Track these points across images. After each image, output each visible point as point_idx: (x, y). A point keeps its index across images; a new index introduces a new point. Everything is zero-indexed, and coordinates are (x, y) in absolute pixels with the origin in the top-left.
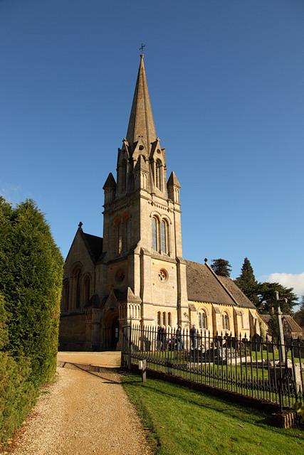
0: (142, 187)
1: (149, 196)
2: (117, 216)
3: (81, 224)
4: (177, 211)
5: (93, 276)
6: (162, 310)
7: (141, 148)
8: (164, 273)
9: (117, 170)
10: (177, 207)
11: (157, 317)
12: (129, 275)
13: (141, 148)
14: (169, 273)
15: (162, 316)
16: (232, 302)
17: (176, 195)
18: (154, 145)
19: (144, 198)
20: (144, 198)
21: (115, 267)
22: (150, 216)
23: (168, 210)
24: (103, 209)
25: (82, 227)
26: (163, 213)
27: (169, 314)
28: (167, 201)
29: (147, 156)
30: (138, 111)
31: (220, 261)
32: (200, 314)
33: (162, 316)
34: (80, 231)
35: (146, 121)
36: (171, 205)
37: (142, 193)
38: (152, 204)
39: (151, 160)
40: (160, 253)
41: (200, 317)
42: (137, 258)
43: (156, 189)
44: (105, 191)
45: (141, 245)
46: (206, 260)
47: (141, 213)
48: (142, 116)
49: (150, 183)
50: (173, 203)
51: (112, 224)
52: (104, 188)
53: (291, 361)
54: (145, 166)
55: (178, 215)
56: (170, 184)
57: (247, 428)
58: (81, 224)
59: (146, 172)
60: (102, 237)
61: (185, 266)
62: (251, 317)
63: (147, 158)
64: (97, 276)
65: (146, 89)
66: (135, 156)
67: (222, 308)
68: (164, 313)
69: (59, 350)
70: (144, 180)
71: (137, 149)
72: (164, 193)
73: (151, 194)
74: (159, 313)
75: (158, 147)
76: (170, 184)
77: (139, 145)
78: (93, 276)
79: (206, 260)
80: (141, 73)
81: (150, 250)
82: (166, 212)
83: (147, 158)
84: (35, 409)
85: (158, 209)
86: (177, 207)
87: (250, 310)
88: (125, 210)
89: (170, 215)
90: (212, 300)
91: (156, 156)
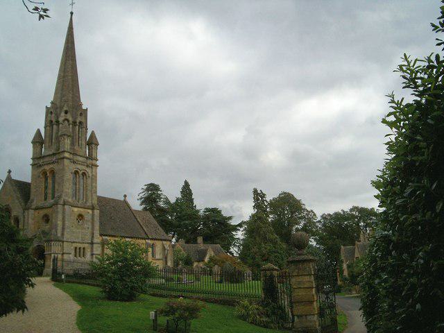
3: (10, 172)
5: (22, 219)
6: (79, 245)
8: (81, 217)
9: (45, 128)
11: (74, 251)
12: (54, 220)
15: (78, 250)
16: (145, 236)
21: (42, 212)
23: (87, 166)
27: (84, 248)
31: (152, 185)
33: (78, 250)
51: (39, 176)
57: (264, 329)
58: (10, 172)
60: (30, 182)
62: (164, 248)
63: (71, 122)
64: (26, 219)
68: (80, 248)
69: (29, 184)
74: (76, 248)
78: (22, 219)
81: (70, 200)
82: (84, 168)
84: (362, 311)
87: (164, 242)
88: (51, 166)
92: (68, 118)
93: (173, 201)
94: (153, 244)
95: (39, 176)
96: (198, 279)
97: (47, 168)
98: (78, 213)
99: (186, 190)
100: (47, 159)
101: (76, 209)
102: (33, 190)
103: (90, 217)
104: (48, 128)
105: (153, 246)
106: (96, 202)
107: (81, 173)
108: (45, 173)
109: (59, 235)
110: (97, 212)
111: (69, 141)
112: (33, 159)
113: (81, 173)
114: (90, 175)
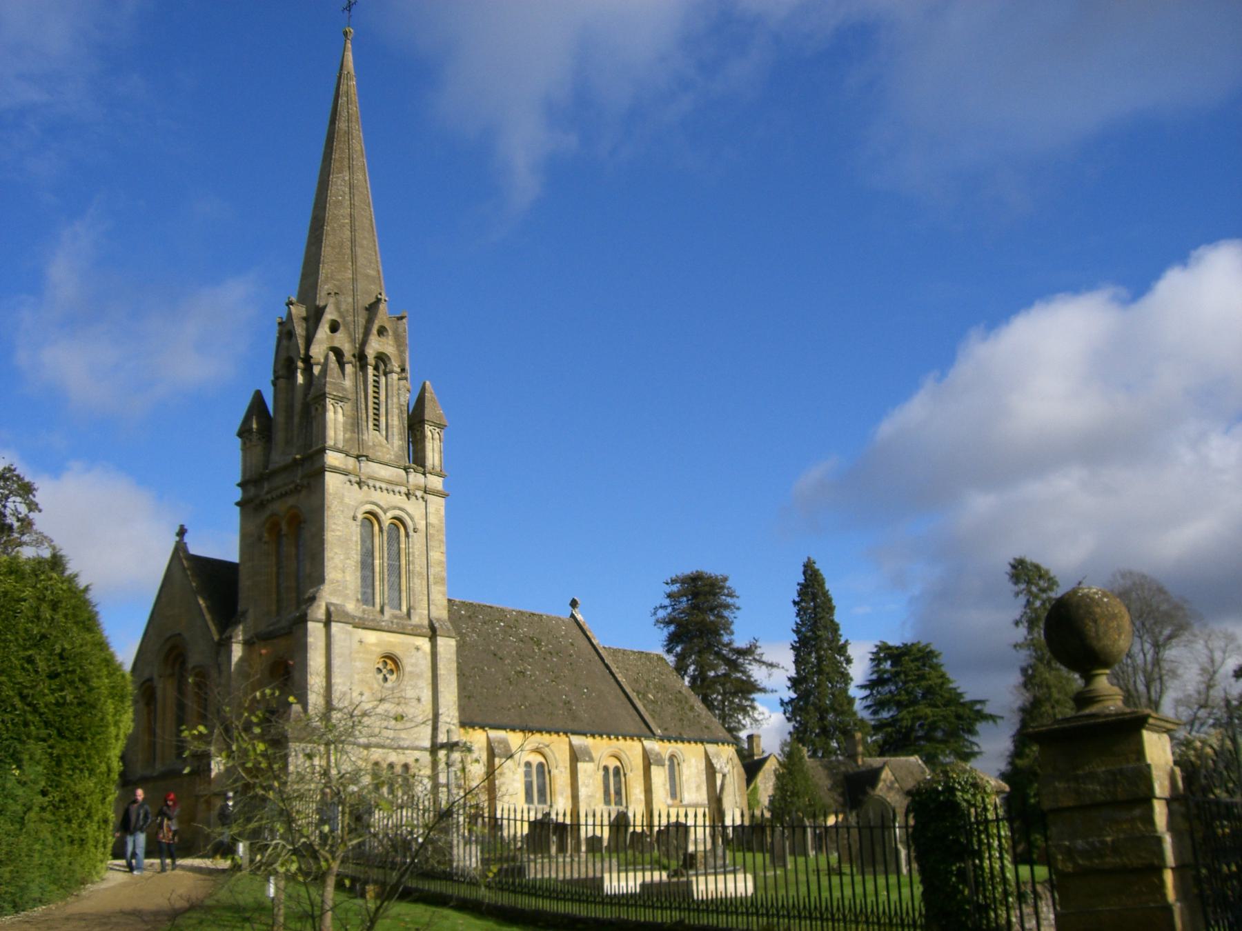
0: (330, 442)
1: (351, 463)
2: (273, 515)
3: (182, 532)
4: (436, 493)
7: (334, 328)
8: (391, 662)
9: (274, 384)
10: (436, 482)
13: (334, 328)
14: (408, 663)
17: (433, 453)
18: (372, 309)
19: (335, 470)
20: (335, 470)
22: (354, 518)
23: (408, 495)
24: (238, 494)
25: (187, 539)
26: (389, 502)
28: (406, 469)
29: (348, 349)
30: (330, 212)
32: (606, 769)
34: (180, 550)
35: (353, 241)
36: (416, 479)
37: (332, 458)
38: (360, 484)
39: (361, 358)
40: (382, 611)
41: (528, 774)
42: (315, 630)
43: (371, 436)
44: (244, 444)
45: (328, 596)
46: (574, 604)
47: (327, 513)
48: (343, 225)
49: (355, 425)
50: (424, 474)
52: (240, 434)
53: (616, 864)
54: (344, 381)
55: (437, 504)
56: (415, 424)
58: (182, 532)
59: (341, 399)
61: (453, 642)
62: (711, 770)
65: (356, 141)
66: (318, 351)
67: (601, 748)
70: (336, 418)
71: (323, 332)
72: (397, 442)
73: (358, 457)
75: (384, 315)
76: (415, 424)
77: (329, 316)
79: (574, 604)
80: (343, 88)
82: (400, 500)
83: (348, 356)
85: (377, 496)
86: (436, 482)
87: (711, 748)
88: (291, 501)
89: (414, 509)
90: (571, 725)
91: (375, 346)
92: (337, 344)
93: (797, 639)
94: (672, 757)
95: (260, 538)
96: (467, 842)
97: (280, 507)
98: (379, 651)
99: (798, 584)
100: (279, 481)
101: (371, 637)
102: (245, 582)
103: (426, 664)
104: (282, 382)
105: (673, 763)
106: (444, 614)
107: (386, 519)
108: (274, 528)
109: (976, 847)
110: (447, 646)
111: (340, 418)
112: (242, 485)
113: (386, 519)
114: (421, 525)
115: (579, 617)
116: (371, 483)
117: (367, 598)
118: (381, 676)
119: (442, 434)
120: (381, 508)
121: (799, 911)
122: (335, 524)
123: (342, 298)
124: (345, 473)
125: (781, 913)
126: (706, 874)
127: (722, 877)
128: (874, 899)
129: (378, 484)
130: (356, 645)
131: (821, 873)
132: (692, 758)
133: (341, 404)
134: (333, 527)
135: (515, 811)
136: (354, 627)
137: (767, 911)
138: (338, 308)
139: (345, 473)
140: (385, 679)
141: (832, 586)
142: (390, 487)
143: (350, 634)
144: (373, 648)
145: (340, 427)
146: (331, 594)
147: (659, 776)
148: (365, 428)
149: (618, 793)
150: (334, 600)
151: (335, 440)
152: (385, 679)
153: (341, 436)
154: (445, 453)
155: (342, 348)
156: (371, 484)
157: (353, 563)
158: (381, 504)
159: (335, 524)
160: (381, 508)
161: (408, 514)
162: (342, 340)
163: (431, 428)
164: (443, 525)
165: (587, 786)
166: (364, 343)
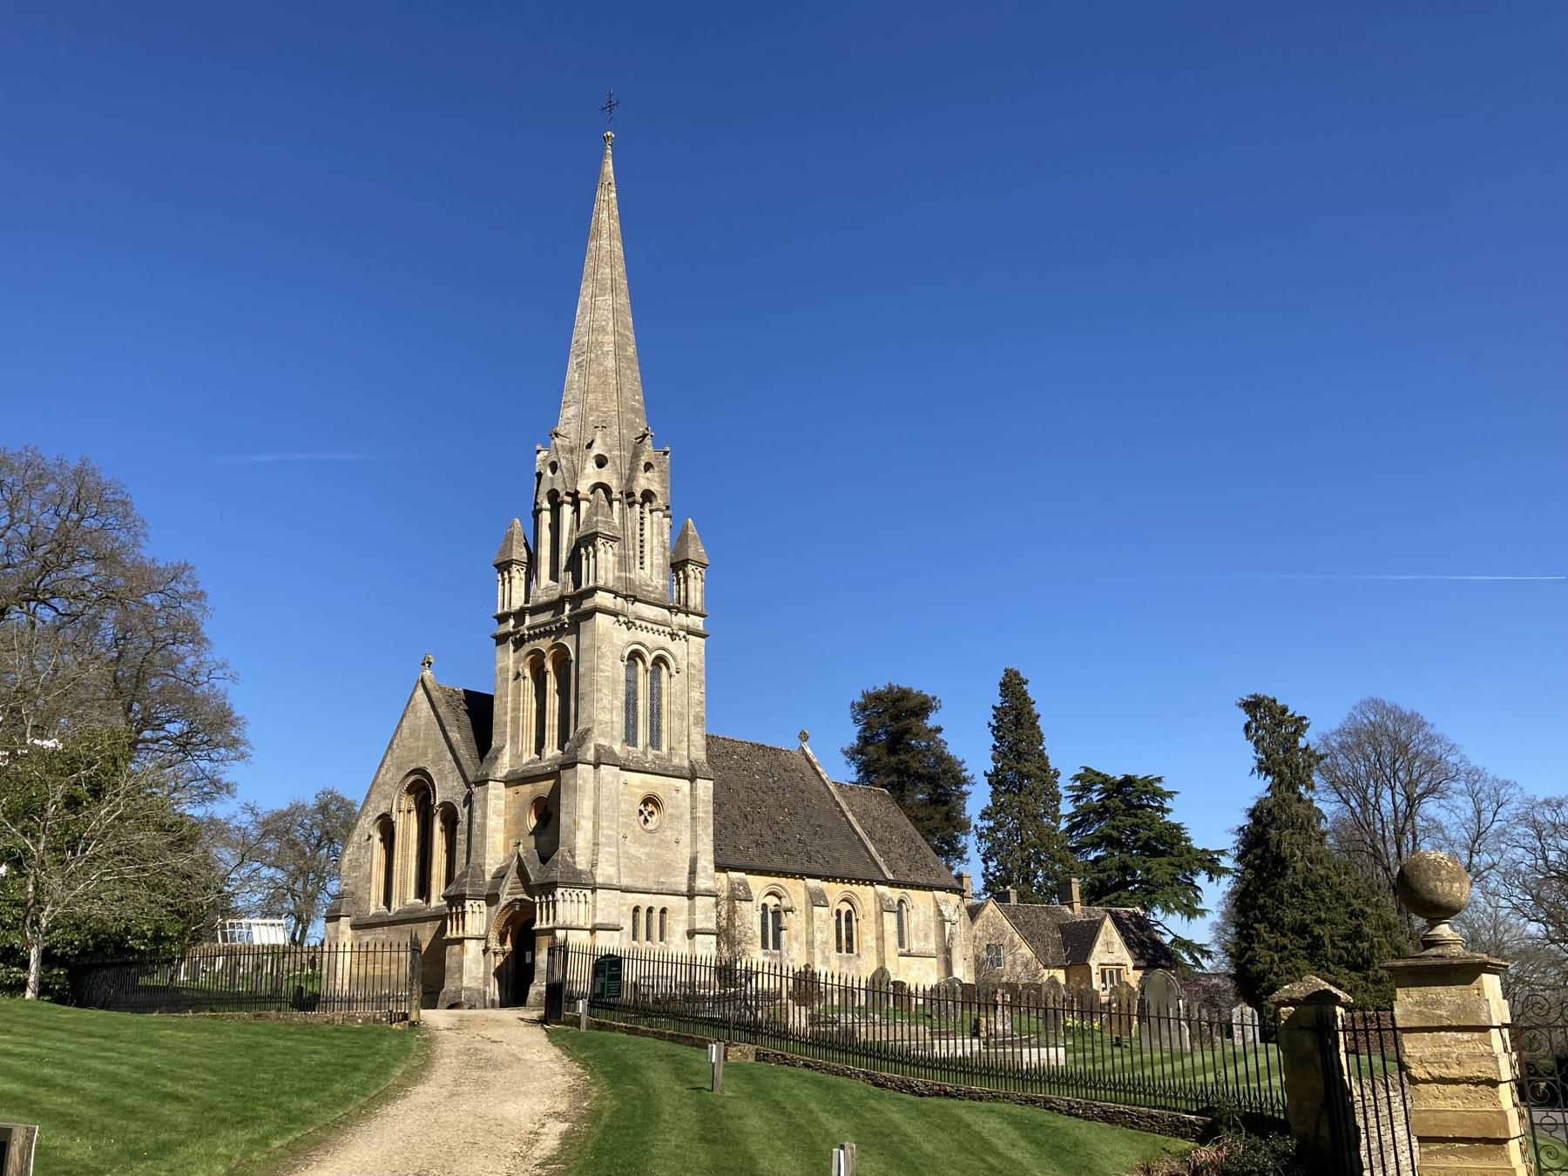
61: (710, 784)
62: (942, 921)
82: (665, 641)
83: (616, 494)
85: (642, 636)
86: (697, 622)
98: (642, 793)
105: (899, 909)
115: (809, 751)
116: (638, 623)
117: (630, 738)
118: (642, 818)
119: (703, 573)
120: (647, 648)
121: (1207, 1096)
122: (604, 664)
123: (607, 431)
124: (615, 614)
125: (1276, 1108)
126: (1056, 1046)
127: (1036, 1050)
128: (1246, 1086)
129: (644, 624)
130: (622, 786)
131: (1105, 1044)
132: (921, 904)
133: (611, 543)
134: (603, 667)
135: (832, 977)
136: (621, 769)
137: (1067, 1080)
138: (604, 443)
139: (615, 614)
140: (646, 821)
141: (1031, 691)
142: (655, 627)
143: (618, 776)
144: (638, 790)
145: (610, 566)
146: (599, 735)
147: (890, 920)
148: (632, 566)
149: (850, 939)
150: (602, 741)
151: (606, 579)
152: (646, 821)
153: (611, 576)
154: (707, 592)
155: (610, 484)
156: (638, 625)
157: (619, 704)
158: (647, 644)
159: (604, 664)
160: (647, 648)
161: (670, 653)
162: (607, 476)
163: (694, 567)
164: (703, 665)
165: (821, 932)
166: (631, 479)
